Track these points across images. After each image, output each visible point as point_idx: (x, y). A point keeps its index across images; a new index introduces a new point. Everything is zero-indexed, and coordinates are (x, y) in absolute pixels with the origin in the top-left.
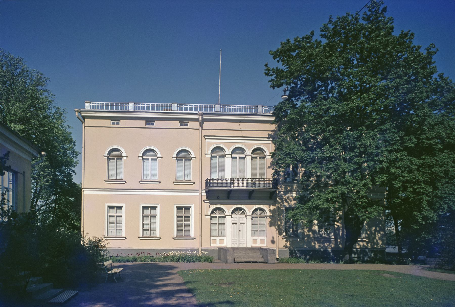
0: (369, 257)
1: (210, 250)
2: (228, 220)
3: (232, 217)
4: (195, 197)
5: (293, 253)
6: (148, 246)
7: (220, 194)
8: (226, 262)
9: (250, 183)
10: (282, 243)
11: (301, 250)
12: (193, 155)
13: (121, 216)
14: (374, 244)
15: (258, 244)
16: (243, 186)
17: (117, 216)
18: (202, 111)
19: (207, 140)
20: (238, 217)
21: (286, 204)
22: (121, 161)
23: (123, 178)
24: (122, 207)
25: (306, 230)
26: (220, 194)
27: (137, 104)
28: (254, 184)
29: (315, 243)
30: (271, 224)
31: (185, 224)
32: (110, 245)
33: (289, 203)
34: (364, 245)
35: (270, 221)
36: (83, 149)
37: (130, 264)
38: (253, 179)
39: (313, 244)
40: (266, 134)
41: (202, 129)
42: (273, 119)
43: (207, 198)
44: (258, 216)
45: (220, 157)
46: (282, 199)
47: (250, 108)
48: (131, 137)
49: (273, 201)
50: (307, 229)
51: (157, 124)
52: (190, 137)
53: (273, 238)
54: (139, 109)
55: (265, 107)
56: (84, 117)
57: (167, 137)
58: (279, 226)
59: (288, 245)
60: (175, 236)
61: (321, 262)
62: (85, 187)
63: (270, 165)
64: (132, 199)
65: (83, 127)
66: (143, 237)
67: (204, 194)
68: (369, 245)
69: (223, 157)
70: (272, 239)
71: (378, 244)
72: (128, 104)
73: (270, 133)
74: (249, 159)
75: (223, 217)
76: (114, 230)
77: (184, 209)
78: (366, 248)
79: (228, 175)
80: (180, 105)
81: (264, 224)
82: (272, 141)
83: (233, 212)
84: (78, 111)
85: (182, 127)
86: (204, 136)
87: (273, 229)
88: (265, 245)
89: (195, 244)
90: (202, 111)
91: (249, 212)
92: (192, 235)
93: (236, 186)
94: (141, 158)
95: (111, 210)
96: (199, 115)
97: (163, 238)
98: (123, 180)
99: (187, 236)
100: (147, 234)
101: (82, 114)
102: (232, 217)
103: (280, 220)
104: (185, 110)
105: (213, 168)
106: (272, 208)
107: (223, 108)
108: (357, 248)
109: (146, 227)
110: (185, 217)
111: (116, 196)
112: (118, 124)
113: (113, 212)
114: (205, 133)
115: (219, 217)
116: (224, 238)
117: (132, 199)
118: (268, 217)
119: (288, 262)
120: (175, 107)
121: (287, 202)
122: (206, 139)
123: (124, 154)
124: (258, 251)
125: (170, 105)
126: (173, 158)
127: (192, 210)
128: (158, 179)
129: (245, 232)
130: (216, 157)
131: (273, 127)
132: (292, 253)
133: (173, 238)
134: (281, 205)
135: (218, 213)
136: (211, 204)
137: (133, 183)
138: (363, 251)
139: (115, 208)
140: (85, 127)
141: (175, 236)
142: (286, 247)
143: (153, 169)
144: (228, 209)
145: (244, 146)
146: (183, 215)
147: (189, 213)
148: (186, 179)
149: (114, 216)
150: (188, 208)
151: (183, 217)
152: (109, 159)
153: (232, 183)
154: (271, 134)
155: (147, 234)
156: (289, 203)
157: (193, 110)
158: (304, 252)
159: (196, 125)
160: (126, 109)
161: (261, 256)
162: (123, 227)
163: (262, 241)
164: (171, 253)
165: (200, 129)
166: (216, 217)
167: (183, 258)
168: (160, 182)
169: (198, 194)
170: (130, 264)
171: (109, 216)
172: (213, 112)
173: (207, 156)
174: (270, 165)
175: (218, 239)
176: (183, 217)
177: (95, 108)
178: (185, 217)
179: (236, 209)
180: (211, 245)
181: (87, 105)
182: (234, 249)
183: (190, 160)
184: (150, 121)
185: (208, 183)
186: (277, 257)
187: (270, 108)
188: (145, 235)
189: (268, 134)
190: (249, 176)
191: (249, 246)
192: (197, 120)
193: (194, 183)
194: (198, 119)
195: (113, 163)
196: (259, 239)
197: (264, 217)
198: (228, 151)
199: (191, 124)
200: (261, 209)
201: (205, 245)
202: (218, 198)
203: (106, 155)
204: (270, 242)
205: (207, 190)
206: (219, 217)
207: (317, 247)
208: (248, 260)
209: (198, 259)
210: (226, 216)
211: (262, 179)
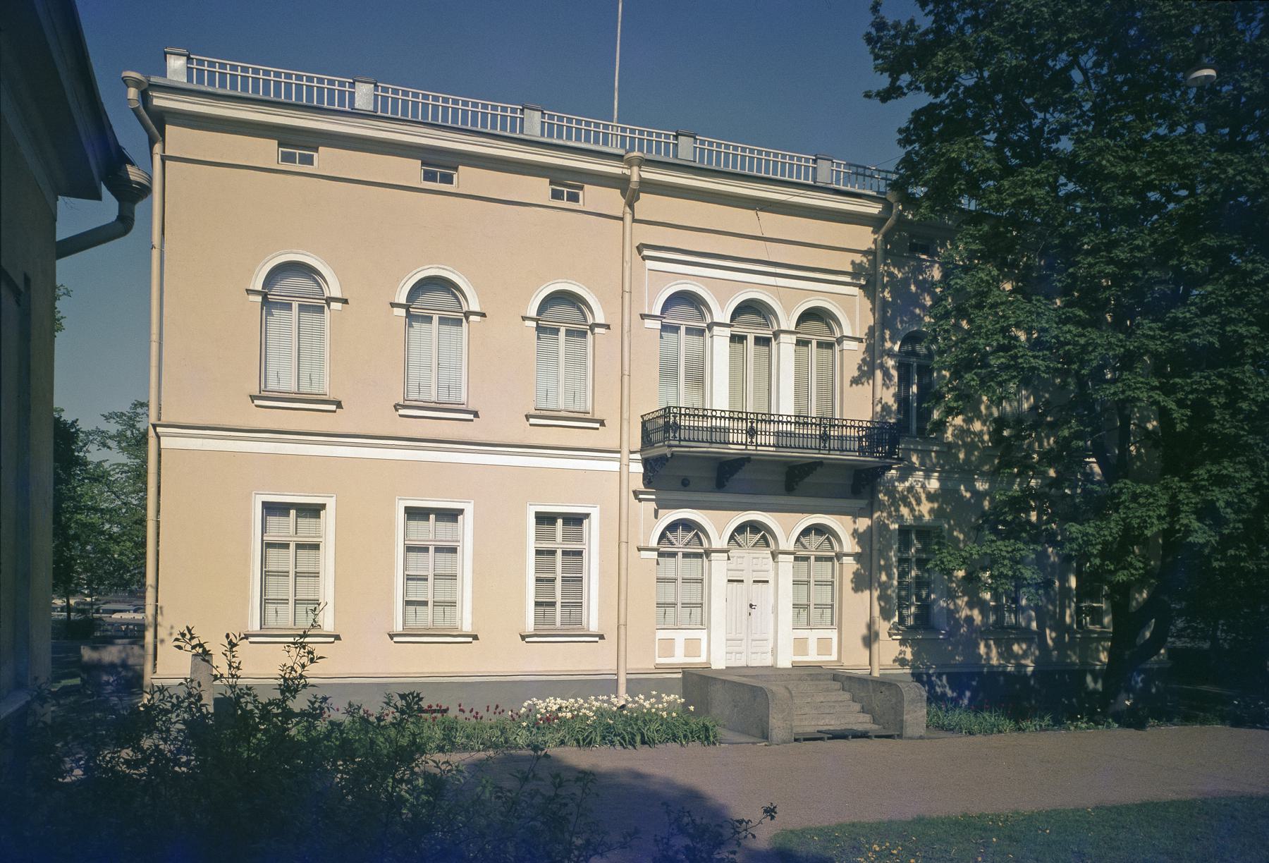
2: (719, 568)
4: (604, 480)
8: (765, 736)
13: (316, 547)
15: (812, 657)
16: (765, 443)
19: (650, 264)
20: (752, 559)
21: (904, 511)
22: (316, 316)
23: (325, 387)
26: (686, 467)
28: (825, 437)
29: (988, 646)
30: (861, 583)
31: (564, 580)
33: (912, 510)
35: (856, 574)
36: (155, 254)
38: (801, 420)
39: (982, 650)
40: (844, 262)
42: (874, 209)
43: (648, 480)
46: (891, 492)
47: (796, 162)
48: (360, 220)
49: (863, 503)
50: (966, 599)
51: (466, 177)
52: (587, 247)
55: (839, 165)
57: (510, 241)
58: (884, 587)
59: (909, 656)
60: (530, 627)
61: (1057, 722)
62: (164, 420)
63: (856, 374)
65: (157, 159)
67: (638, 468)
72: (352, 85)
73: (858, 258)
74: (786, 346)
77: (560, 522)
80: (551, 117)
82: (861, 287)
84: (137, 83)
86: (640, 248)
91: (787, 541)
92: (593, 623)
93: (737, 443)
94: (403, 312)
95: (273, 520)
98: (471, 408)
99: (574, 630)
100: (426, 616)
101: (156, 102)
103: (888, 569)
105: (668, 372)
106: (863, 523)
110: (565, 553)
112: (308, 160)
113: (284, 528)
115: (686, 555)
116: (702, 634)
117: (362, 479)
118: (848, 560)
121: (908, 505)
122: (644, 258)
124: (838, 685)
126: (528, 323)
127: (593, 528)
128: (464, 399)
129: (777, 610)
131: (865, 238)
133: (523, 638)
134: (890, 515)
136: (662, 505)
139: (293, 512)
140: (164, 159)
141: (530, 627)
142: (902, 662)
144: (718, 524)
145: (775, 295)
147: (580, 539)
148: (305, 388)
149: (286, 546)
150: (575, 520)
151: (559, 553)
154: (860, 264)
155: (426, 616)
156: (912, 510)
159: (611, 199)
161: (857, 707)
162: (327, 590)
163: (824, 644)
165: (628, 218)
166: (673, 555)
168: (339, 405)
169: (615, 466)
172: (671, 159)
174: (856, 374)
175: (680, 637)
176: (559, 553)
181: (176, 65)
183: (320, 310)
184: (439, 165)
187: (859, 171)
189: (853, 263)
190: (786, 406)
191: (785, 662)
195: (286, 322)
196: (813, 636)
201: (642, 661)
202: (685, 484)
203: (259, 287)
210: (708, 553)
211: (826, 422)
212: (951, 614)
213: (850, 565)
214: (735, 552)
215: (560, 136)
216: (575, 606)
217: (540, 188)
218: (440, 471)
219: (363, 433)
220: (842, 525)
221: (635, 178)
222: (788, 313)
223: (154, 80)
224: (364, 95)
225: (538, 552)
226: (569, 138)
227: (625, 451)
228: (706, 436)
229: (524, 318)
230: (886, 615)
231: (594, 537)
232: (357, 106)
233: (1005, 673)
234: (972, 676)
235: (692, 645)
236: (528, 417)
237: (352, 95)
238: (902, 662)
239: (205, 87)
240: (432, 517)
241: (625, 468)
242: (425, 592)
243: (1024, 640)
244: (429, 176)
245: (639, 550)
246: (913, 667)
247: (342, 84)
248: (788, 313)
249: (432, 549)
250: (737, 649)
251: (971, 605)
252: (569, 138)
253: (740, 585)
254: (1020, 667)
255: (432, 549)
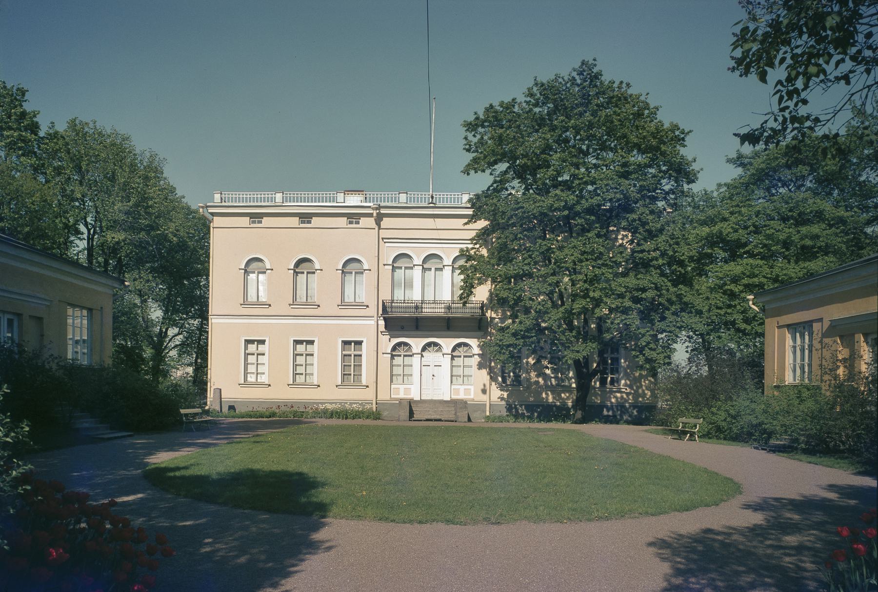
0: (630, 416)
3: (422, 356)
4: (368, 328)
5: (512, 408)
6: (309, 398)
7: (404, 323)
10: (496, 394)
11: (527, 406)
12: (366, 267)
14: (639, 396)
17: (307, 355)
24: (362, 341)
25: (533, 374)
26: (404, 323)
29: (547, 394)
30: (480, 366)
34: (622, 397)
37: (265, 419)
39: (544, 395)
41: (379, 228)
43: (386, 328)
44: (462, 354)
45: (406, 268)
48: (281, 241)
53: (484, 385)
59: (505, 396)
64: (279, 331)
66: (246, 383)
67: (382, 323)
68: (631, 397)
69: (411, 268)
70: (482, 387)
71: (644, 395)
75: (411, 356)
76: (253, 373)
78: (626, 401)
79: (416, 295)
81: (471, 367)
83: (424, 349)
85: (252, 225)
86: (383, 239)
87: (484, 372)
88: (472, 397)
89: (368, 395)
92: (364, 382)
93: (427, 311)
96: (373, 209)
97: (325, 388)
102: (422, 356)
108: (612, 403)
109: (300, 370)
110: (355, 355)
112: (260, 222)
113: (301, 348)
114: (383, 234)
123: (317, 266)
128: (364, 300)
129: (448, 377)
130: (430, 269)
132: (509, 408)
135: (401, 351)
136: (392, 336)
137: (330, 306)
138: (621, 406)
142: (502, 399)
143: (260, 286)
144: (417, 343)
146: (352, 352)
149: (302, 355)
150: (359, 343)
152: (296, 273)
158: (530, 408)
162: (315, 370)
163: (467, 391)
164: (321, 407)
165: (377, 229)
166: (400, 356)
167: (337, 412)
170: (265, 419)
171: (296, 355)
173: (386, 267)
178: (355, 355)
179: (429, 345)
181: (217, 197)
183: (362, 273)
184: (306, 218)
186: (488, 414)
188: (298, 380)
192: (370, 215)
193: (368, 306)
197: (471, 357)
198: (418, 260)
199: (363, 221)
200: (466, 345)
201: (383, 396)
202: (403, 328)
204: (480, 392)
206: (465, 356)
207: (550, 399)
208: (429, 417)
209: (357, 415)
212: (528, 380)
213: (477, 359)
218: (305, 327)
220: (474, 343)
230: (493, 379)
233: (555, 406)
234: (538, 406)
235: (407, 391)
238: (502, 399)
239: (252, 204)
243: (568, 392)
246: (507, 402)
251: (538, 376)
254: (566, 404)
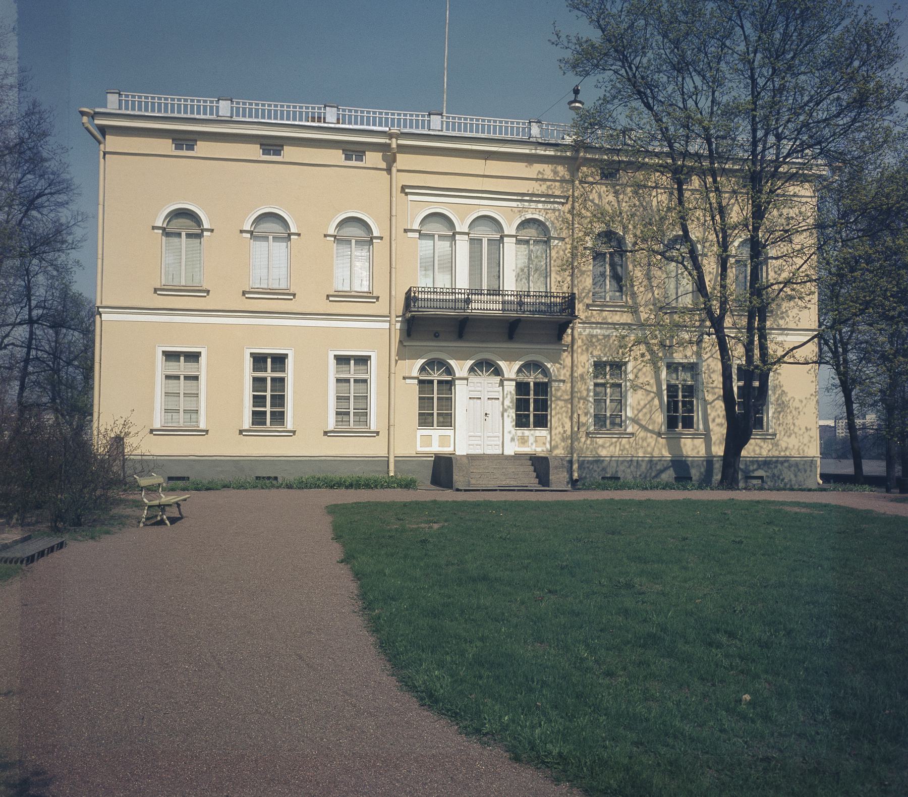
1: (414, 461)
4: (376, 336)
9: (511, 302)
18: (399, 126)
19: (410, 197)
26: (435, 330)
27: (238, 103)
28: (521, 303)
32: (458, 452)
36: (101, 207)
48: (225, 184)
52: (361, 189)
54: (250, 116)
56: (103, 130)
57: (318, 188)
62: (104, 304)
72: (218, 102)
77: (352, 362)
86: (403, 188)
90: (399, 126)
104: (356, 123)
107: (448, 123)
110: (356, 381)
111: (185, 330)
119: (255, 487)
120: (331, 115)
122: (407, 194)
123: (206, 225)
125: (319, 108)
126: (245, 235)
140: (105, 153)
141: (331, 425)
146: (269, 374)
150: (363, 360)
151: (435, 382)
153: (468, 301)
155: (181, 420)
157: (376, 122)
160: (211, 114)
169: (387, 325)
176: (435, 382)
177: (166, 111)
180: (420, 449)
181: (113, 99)
182: (471, 458)
185: (410, 299)
194: (389, 145)
201: (401, 449)
202: (436, 336)
205: (409, 315)
214: (473, 379)
215: (205, 114)
216: (362, 415)
217: (337, 156)
219: (200, 308)
221: (394, 145)
222: (462, 221)
223: (97, 110)
224: (225, 108)
225: (338, 381)
226: (153, 110)
227: (393, 316)
228: (451, 305)
229: (242, 232)
231: (375, 372)
232: (220, 114)
236: (328, 296)
237: (217, 107)
240: (182, 358)
241: (393, 327)
242: (183, 403)
244: (348, 158)
245: (404, 378)
247: (212, 102)
248: (462, 221)
249: (182, 378)
250: (495, 443)
252: (166, 111)
253: (479, 401)
255: (182, 378)
